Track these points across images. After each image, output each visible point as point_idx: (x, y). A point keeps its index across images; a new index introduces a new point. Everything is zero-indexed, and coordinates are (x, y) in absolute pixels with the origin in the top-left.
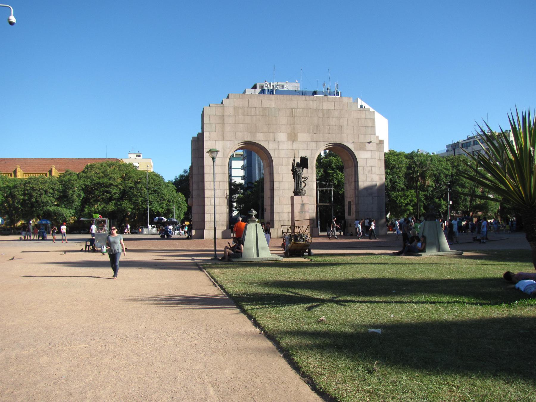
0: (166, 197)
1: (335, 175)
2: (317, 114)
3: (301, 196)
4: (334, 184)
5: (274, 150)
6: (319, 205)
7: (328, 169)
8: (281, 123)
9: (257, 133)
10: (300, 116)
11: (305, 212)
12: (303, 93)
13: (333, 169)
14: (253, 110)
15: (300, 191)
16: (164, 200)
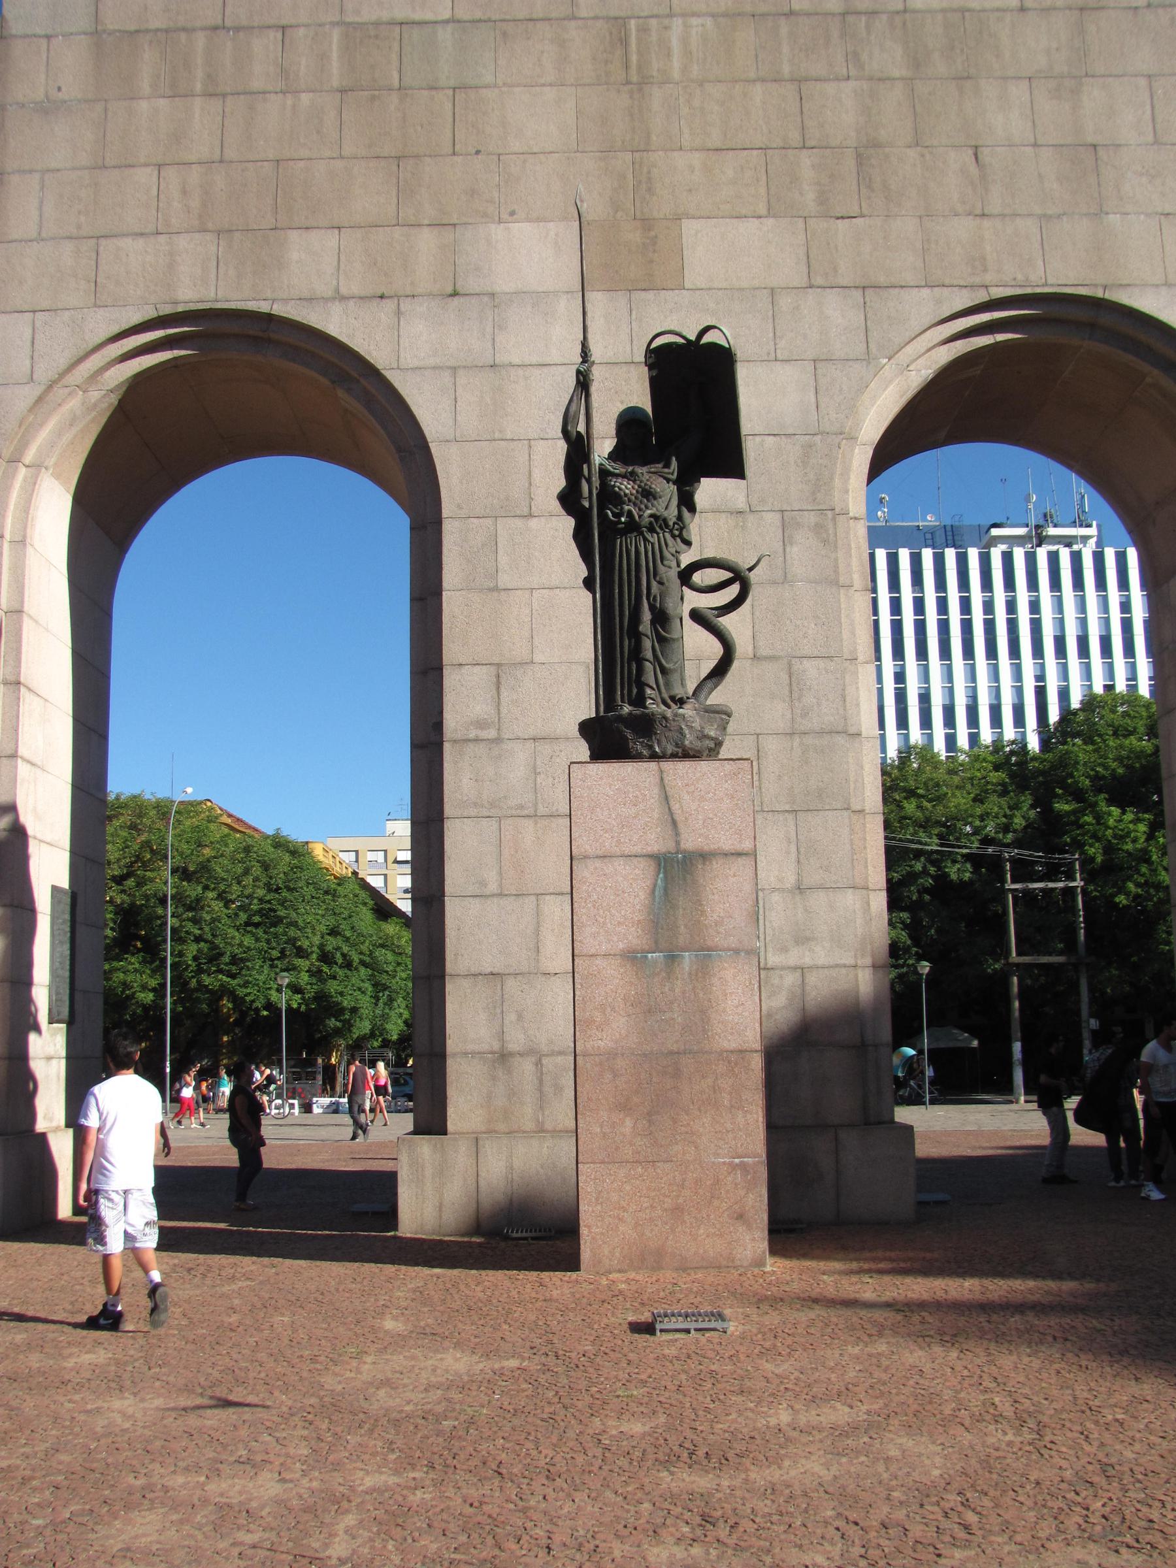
0: (311, 941)
1: (1088, 819)
2: (854, 57)
3: (653, 765)
4: (1087, 861)
5: (446, 376)
6: (1017, 965)
7: (1057, 796)
8: (516, 146)
9: (294, 235)
10: (695, 71)
11: (706, 954)
12: (949, 533)
13: (1077, 795)
14: (264, 47)
15: (654, 707)
16: (301, 953)
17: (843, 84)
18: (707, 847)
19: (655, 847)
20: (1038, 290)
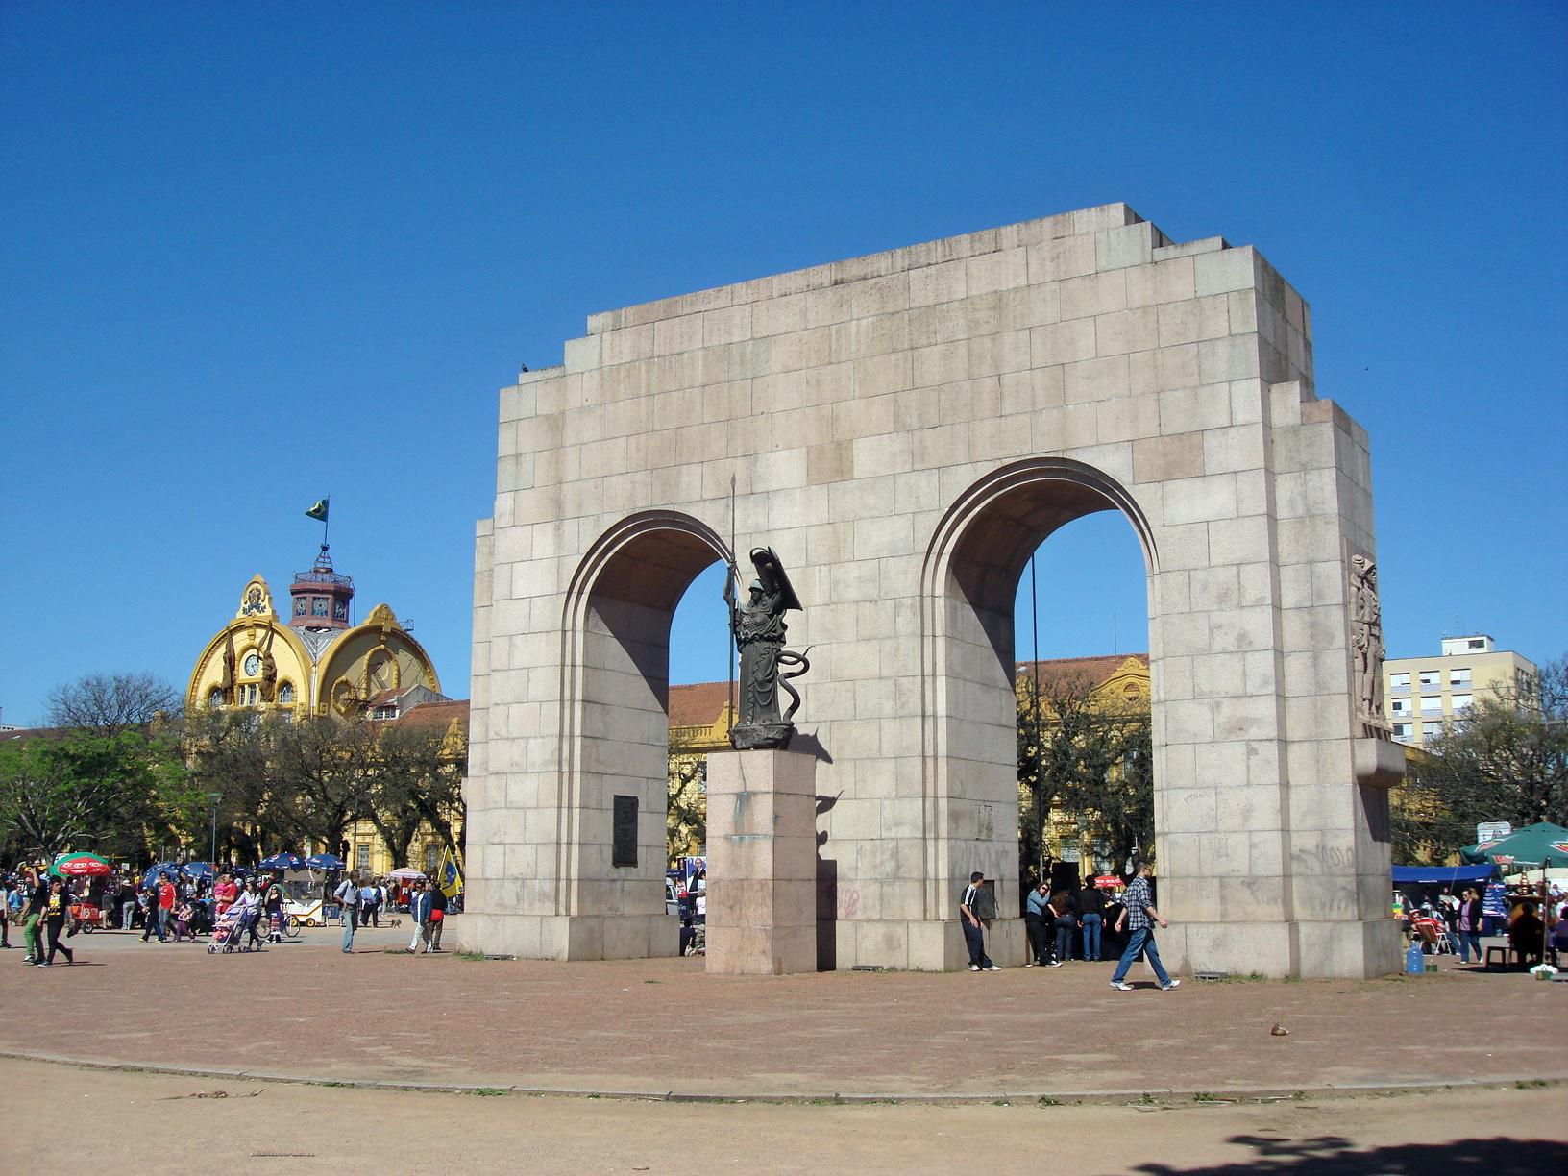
17: (933, 347)
18: (756, 790)
19: (736, 791)
20: (1028, 458)
